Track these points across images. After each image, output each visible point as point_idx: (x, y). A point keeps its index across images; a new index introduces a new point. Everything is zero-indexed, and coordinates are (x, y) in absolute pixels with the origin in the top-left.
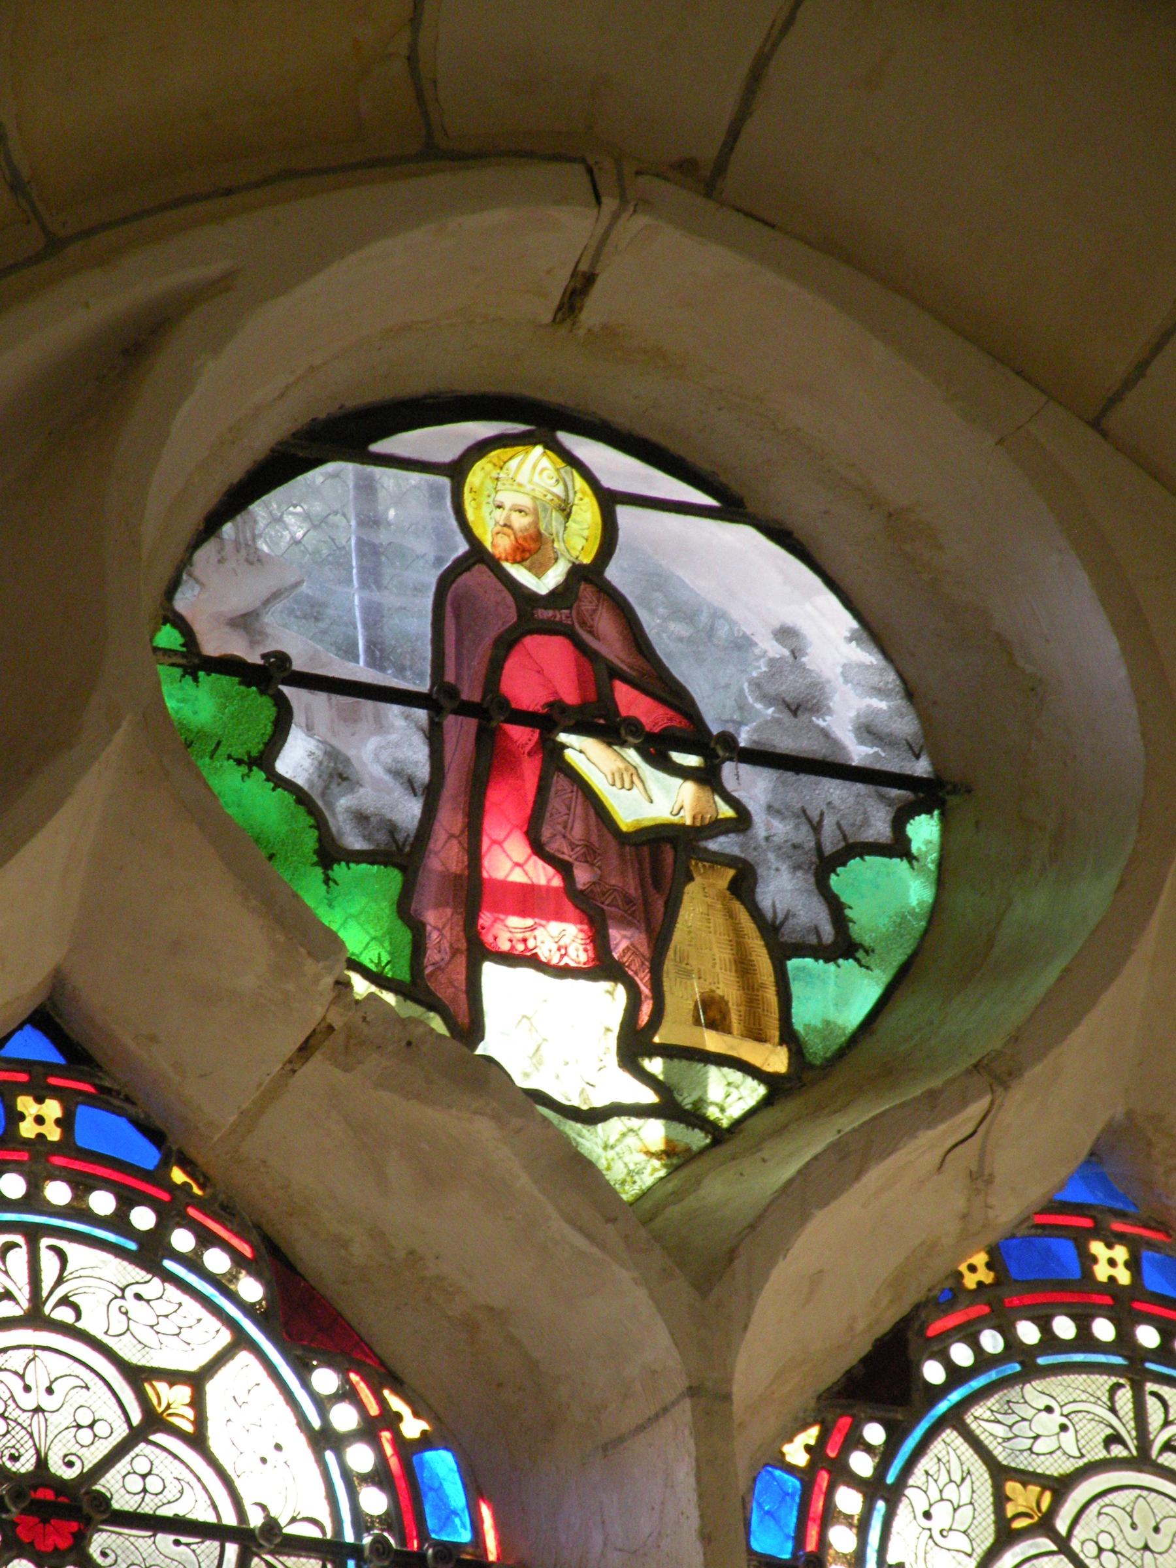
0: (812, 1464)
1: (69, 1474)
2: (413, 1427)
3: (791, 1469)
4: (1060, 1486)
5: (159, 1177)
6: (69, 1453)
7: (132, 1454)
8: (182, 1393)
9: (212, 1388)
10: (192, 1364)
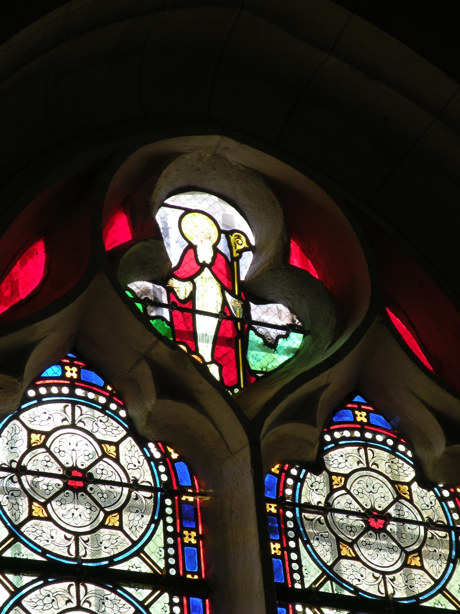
0: (280, 473)
1: (82, 468)
2: (175, 456)
3: (274, 474)
4: (347, 476)
5: (104, 388)
6: (83, 462)
7: (96, 506)
8: (113, 448)
9: (121, 446)
10: (115, 440)
